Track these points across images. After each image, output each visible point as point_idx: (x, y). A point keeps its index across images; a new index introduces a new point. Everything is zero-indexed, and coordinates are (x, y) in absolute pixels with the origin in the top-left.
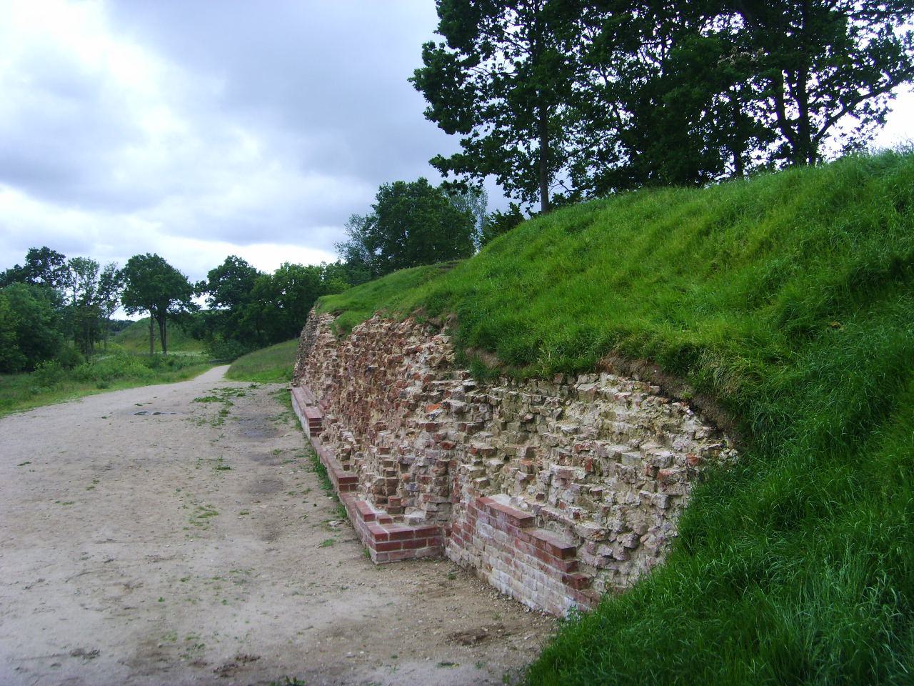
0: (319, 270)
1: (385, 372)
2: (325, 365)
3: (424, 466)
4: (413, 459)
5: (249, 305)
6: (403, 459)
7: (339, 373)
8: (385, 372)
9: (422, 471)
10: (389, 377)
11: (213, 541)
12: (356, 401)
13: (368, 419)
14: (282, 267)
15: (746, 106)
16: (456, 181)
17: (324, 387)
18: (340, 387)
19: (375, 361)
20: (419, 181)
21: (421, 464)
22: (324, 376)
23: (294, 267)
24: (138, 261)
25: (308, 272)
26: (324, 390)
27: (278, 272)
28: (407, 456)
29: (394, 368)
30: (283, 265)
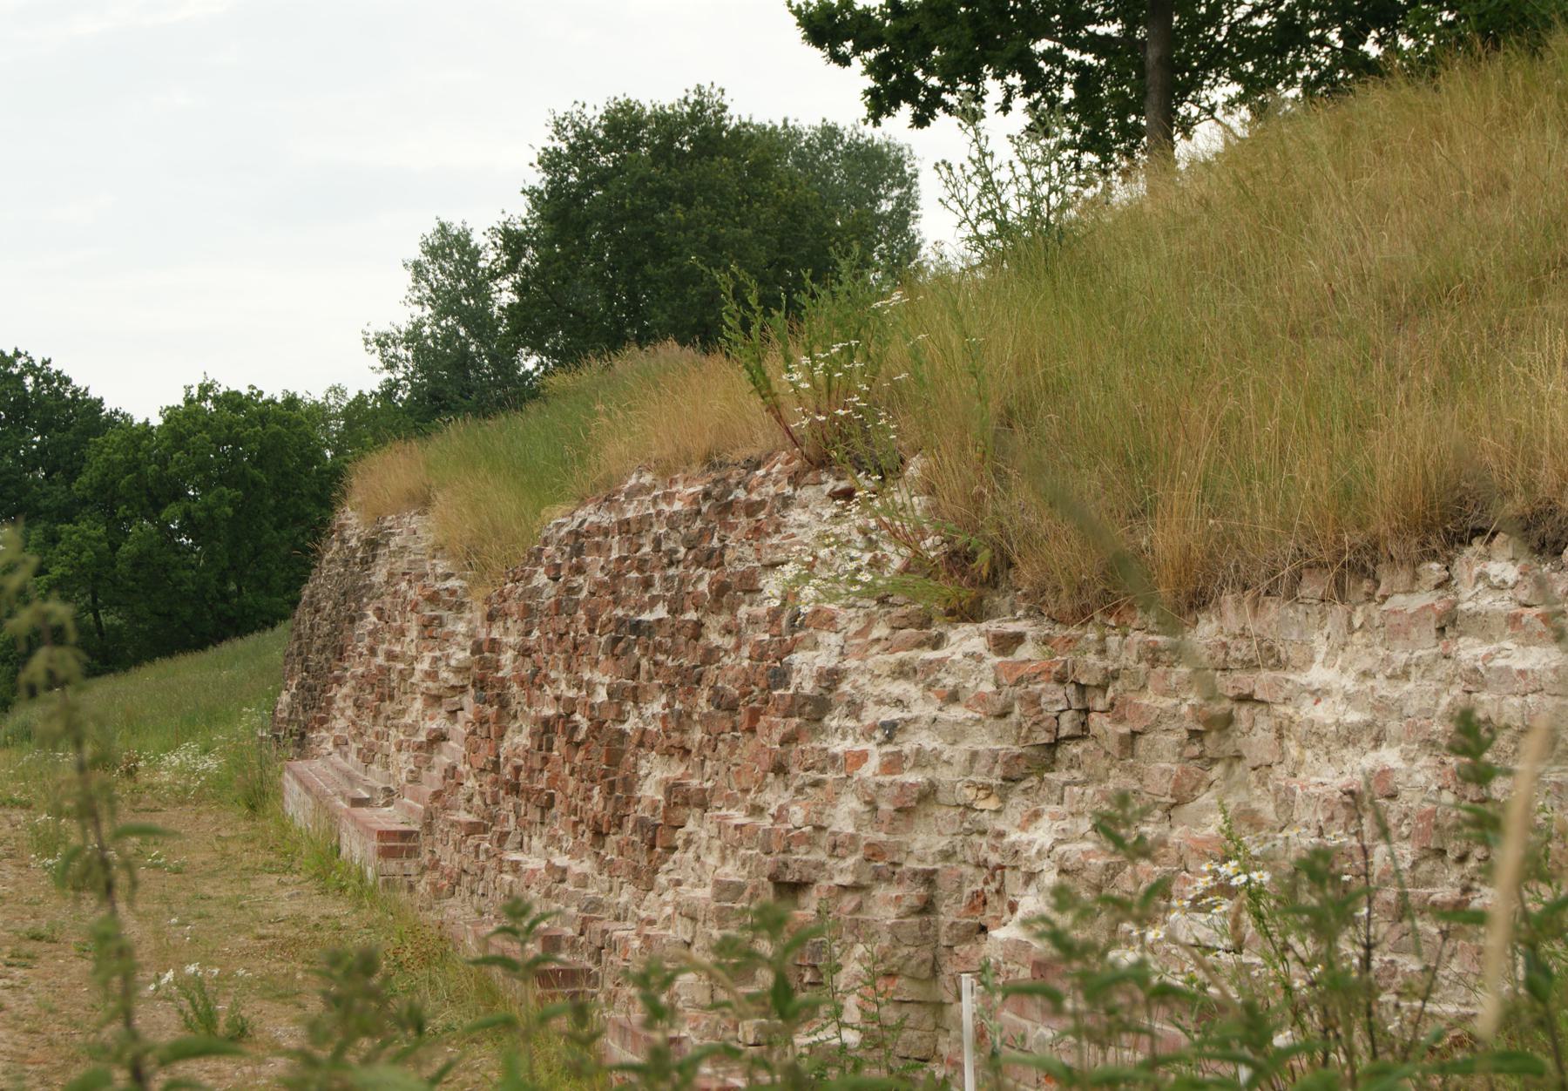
0: (319, 413)
1: (699, 625)
2: (424, 665)
3: (856, 888)
4: (820, 866)
5: (67, 527)
6: (786, 865)
7: (498, 669)
8: (699, 625)
9: (849, 901)
10: (714, 638)
11: (1388, 99)
12: (580, 736)
13: (629, 784)
14: (189, 401)
15: (752, 360)
16: (920, 121)
17: (422, 737)
18: (499, 717)
19: (654, 601)
20: (546, 168)
21: (847, 879)
22: (418, 704)
23: (232, 401)
24: (761, 169)
25: (281, 420)
26: (420, 747)
27: (172, 415)
28: (801, 854)
29: (733, 609)
30: (195, 392)
